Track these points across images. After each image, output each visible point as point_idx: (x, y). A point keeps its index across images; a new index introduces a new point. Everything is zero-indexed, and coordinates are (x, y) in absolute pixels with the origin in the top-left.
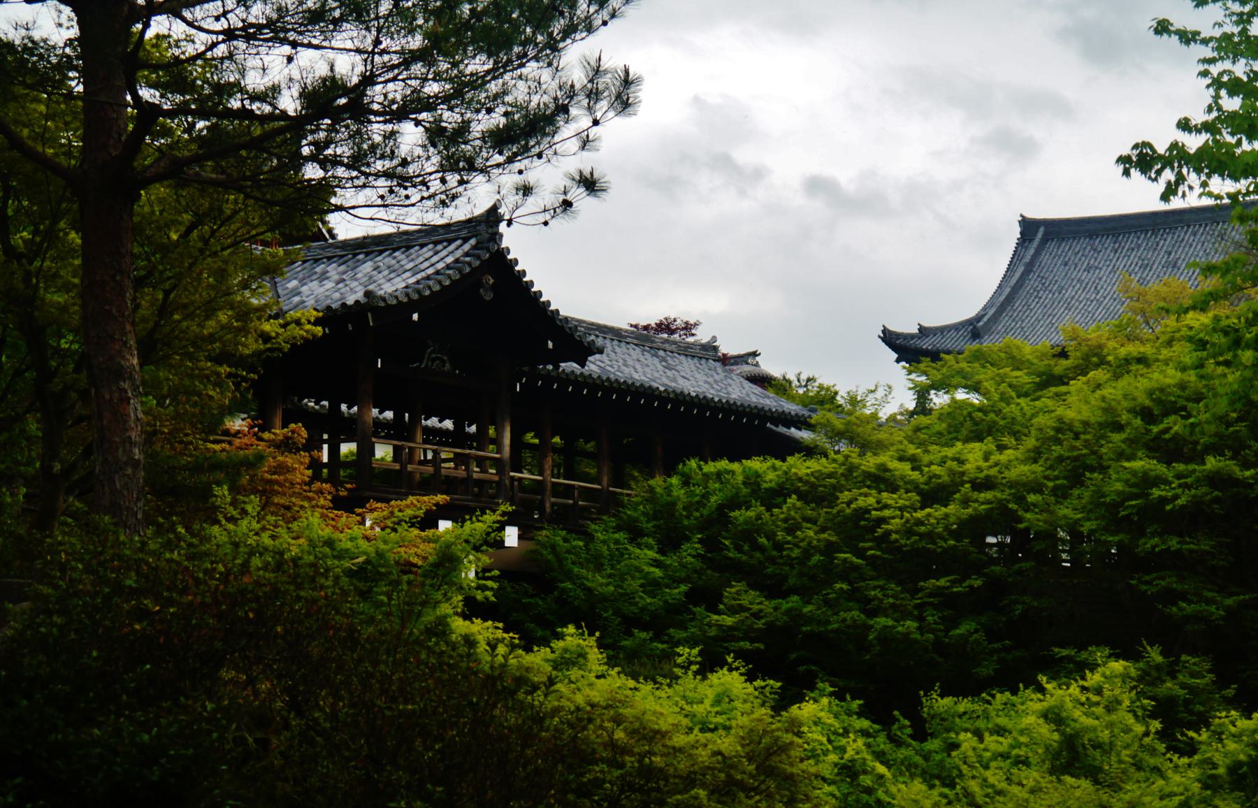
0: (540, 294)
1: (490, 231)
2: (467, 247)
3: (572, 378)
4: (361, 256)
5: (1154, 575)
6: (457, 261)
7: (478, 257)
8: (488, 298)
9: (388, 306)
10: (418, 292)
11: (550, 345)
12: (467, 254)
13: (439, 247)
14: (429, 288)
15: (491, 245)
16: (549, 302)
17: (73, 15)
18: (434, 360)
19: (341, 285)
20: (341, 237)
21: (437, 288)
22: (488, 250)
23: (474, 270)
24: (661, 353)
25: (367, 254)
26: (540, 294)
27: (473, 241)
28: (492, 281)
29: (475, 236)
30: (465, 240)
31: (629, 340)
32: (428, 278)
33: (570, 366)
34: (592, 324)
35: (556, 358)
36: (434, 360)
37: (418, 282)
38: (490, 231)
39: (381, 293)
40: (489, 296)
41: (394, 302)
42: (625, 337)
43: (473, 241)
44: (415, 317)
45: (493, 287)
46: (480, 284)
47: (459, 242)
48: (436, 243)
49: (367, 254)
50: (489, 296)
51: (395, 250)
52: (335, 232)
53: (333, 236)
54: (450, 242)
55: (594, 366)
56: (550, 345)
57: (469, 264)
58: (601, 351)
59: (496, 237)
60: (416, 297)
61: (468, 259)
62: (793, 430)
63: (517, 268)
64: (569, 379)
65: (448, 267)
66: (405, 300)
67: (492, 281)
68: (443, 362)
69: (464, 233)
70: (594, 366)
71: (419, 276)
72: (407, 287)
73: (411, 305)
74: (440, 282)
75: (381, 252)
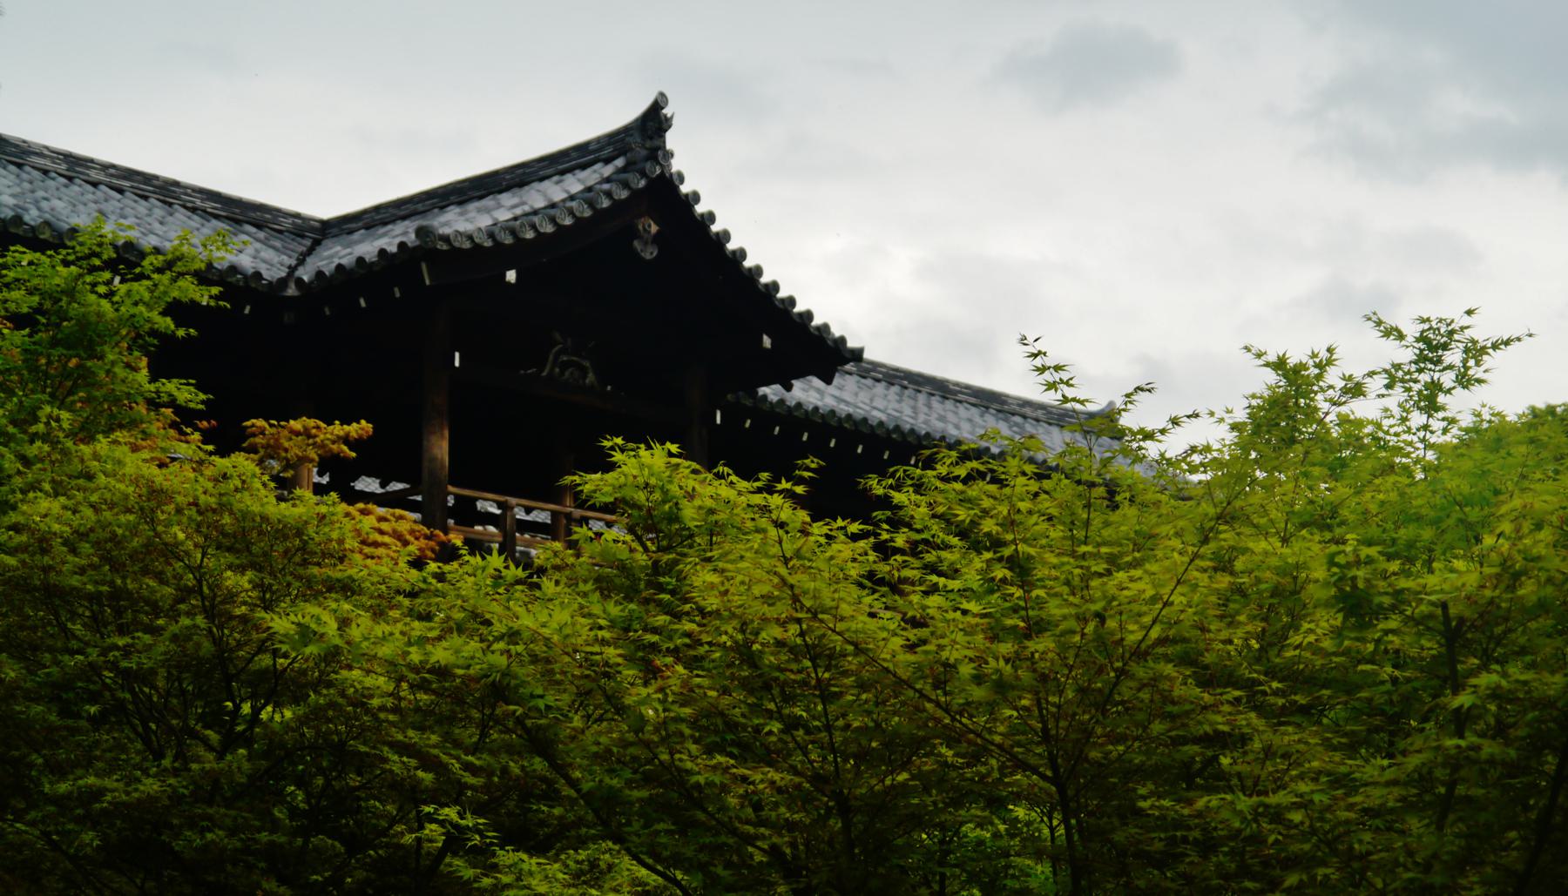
0: (725, 236)
1: (648, 144)
2: (608, 170)
3: (833, 423)
7: (626, 185)
8: (648, 256)
10: (513, 232)
11: (767, 342)
12: (608, 180)
14: (533, 227)
15: (648, 165)
16: (696, 197)
17: (695, 465)
18: (565, 366)
22: (643, 174)
23: (617, 205)
24: (1018, 419)
26: (725, 236)
27: (620, 162)
28: (654, 229)
31: (961, 397)
34: (897, 370)
36: (565, 366)
38: (648, 144)
39: (446, 231)
41: (467, 245)
42: (955, 393)
43: (620, 162)
44: (511, 276)
45: (656, 239)
50: (650, 253)
56: (767, 342)
57: (608, 194)
59: (659, 154)
60: (508, 240)
61: (606, 186)
63: (797, 310)
67: (654, 229)
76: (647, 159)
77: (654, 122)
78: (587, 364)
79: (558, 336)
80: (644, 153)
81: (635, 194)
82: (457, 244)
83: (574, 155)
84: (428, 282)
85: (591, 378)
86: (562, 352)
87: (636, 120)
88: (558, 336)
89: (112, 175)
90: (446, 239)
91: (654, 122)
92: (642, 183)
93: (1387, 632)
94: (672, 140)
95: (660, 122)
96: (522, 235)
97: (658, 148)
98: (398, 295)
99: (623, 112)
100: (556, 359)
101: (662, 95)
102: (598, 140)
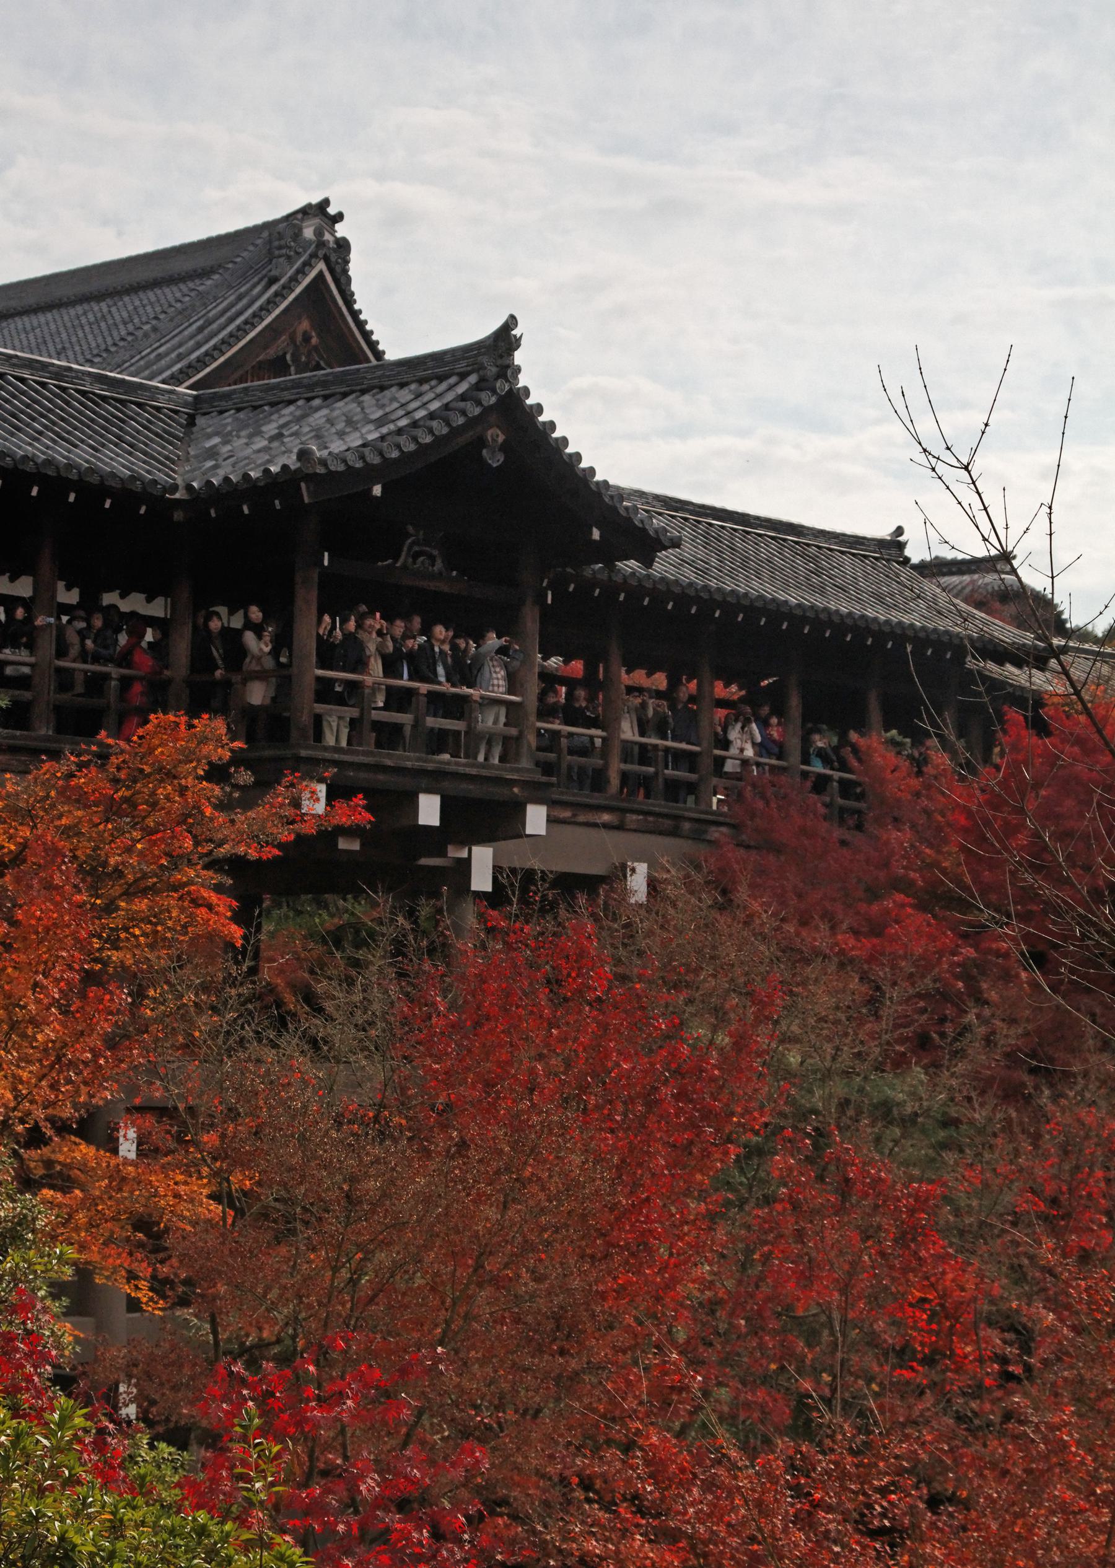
2: (462, 388)
4: (317, 402)
5: (432, 585)
6: (446, 407)
9: (331, 474)
13: (426, 387)
19: (275, 444)
20: (391, 355)
21: (412, 447)
25: (325, 398)
27: (473, 379)
28: (501, 438)
29: (477, 371)
30: (463, 376)
32: (400, 431)
33: (630, 566)
35: (608, 554)
36: (416, 556)
37: (382, 438)
40: (496, 460)
41: (341, 468)
43: (473, 379)
45: (504, 448)
46: (481, 442)
47: (453, 380)
48: (421, 381)
49: (325, 398)
50: (496, 460)
51: (363, 392)
52: (381, 347)
53: (379, 355)
54: (441, 379)
55: (664, 566)
58: (676, 544)
59: (509, 371)
61: (462, 404)
62: (1009, 667)
64: (636, 589)
65: (432, 416)
66: (359, 465)
68: (432, 558)
69: (461, 367)
70: (664, 566)
71: (384, 430)
72: (364, 445)
73: (370, 473)
74: (415, 439)
75: (345, 395)
76: (498, 377)
77: (505, 340)
78: (435, 552)
79: (410, 529)
80: (494, 370)
81: (487, 410)
82: (333, 468)
83: (430, 364)
84: (306, 500)
85: (439, 565)
86: (413, 543)
87: (488, 337)
88: (410, 529)
89: (14, 365)
90: (323, 462)
91: (505, 340)
92: (493, 400)
93: (744, 1422)
94: (519, 357)
95: (511, 343)
96: (388, 456)
97: (508, 366)
98: (277, 502)
99: (478, 328)
100: (409, 549)
101: (513, 317)
102: (453, 351)
